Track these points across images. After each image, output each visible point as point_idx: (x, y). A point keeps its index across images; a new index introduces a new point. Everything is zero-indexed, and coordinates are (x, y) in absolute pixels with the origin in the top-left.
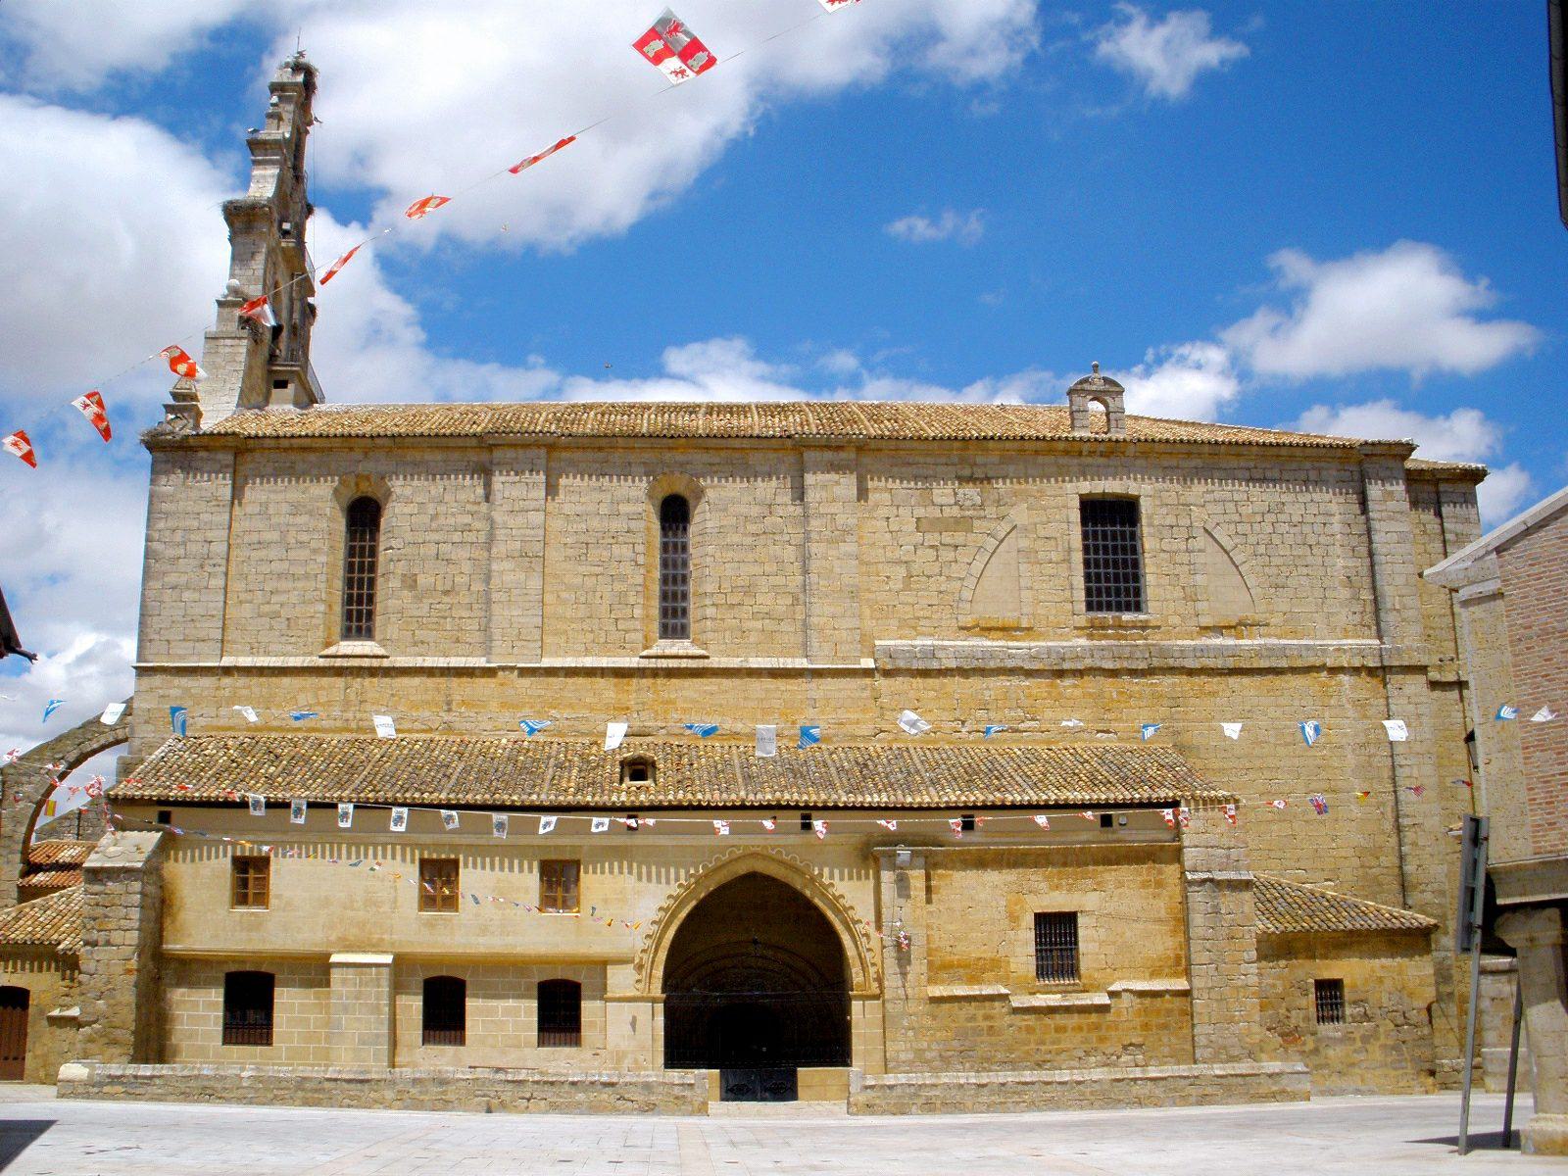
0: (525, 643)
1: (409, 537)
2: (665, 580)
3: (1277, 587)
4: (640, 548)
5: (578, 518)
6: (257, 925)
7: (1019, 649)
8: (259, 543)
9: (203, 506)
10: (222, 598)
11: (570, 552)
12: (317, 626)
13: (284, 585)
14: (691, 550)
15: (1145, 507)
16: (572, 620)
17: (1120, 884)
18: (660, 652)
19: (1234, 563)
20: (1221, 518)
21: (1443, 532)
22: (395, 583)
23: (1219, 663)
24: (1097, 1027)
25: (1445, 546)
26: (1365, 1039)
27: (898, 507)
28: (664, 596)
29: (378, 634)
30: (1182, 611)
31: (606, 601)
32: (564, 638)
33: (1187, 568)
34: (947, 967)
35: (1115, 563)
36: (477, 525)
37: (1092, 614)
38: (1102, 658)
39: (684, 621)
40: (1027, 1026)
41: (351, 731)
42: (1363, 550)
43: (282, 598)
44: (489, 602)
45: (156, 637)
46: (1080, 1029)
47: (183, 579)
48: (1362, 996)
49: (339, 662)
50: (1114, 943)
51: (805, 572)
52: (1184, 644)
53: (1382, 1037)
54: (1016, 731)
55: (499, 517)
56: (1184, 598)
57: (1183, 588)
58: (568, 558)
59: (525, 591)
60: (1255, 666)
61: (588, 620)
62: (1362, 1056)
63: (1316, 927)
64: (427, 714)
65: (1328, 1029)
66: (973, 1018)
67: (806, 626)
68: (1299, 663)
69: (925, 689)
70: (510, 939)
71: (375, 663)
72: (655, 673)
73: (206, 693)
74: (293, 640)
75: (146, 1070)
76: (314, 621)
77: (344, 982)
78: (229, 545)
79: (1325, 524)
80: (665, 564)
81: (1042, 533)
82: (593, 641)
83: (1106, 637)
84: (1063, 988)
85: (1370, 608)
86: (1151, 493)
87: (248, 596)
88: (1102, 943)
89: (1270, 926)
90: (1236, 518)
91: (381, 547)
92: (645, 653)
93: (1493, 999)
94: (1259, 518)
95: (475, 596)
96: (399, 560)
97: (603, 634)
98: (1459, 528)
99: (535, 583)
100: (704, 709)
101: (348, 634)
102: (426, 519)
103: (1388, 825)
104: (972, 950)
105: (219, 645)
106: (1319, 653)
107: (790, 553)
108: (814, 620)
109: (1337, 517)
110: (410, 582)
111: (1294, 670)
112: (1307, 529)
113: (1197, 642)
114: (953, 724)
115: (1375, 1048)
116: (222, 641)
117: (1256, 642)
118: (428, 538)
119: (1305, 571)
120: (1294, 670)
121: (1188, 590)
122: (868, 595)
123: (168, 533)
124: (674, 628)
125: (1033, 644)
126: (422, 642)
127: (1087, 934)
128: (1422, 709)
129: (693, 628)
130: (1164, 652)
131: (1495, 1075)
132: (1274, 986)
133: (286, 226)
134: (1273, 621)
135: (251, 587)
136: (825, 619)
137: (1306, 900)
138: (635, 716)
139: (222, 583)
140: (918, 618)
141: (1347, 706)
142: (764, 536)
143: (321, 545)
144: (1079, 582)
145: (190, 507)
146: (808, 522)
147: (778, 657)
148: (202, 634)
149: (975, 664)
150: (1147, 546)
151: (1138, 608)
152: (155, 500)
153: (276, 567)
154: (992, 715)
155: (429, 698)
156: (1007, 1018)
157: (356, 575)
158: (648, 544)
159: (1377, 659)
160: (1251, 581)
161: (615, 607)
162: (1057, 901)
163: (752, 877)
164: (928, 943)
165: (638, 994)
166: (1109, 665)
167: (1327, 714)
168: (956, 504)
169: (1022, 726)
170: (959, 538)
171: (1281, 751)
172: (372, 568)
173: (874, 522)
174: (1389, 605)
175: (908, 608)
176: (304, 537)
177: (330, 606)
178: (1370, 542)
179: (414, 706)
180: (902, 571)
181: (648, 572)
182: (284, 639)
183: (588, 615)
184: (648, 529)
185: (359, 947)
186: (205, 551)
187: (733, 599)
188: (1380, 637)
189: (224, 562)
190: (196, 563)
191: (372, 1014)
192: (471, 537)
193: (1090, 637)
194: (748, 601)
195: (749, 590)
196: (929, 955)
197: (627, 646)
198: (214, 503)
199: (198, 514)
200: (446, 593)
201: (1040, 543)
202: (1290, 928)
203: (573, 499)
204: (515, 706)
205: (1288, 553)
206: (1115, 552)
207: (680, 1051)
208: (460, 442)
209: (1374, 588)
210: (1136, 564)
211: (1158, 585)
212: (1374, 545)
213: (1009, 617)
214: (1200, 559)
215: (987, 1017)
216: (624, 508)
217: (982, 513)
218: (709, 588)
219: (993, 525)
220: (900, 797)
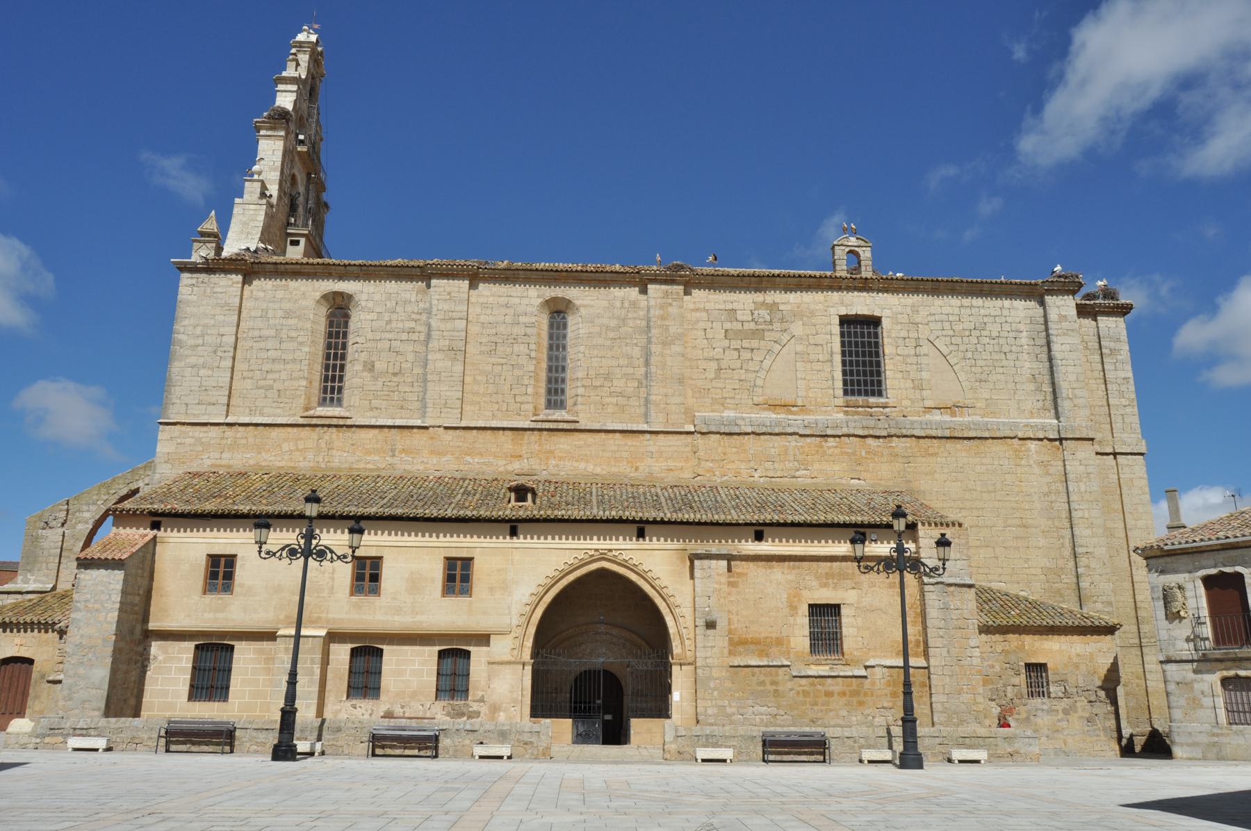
0: (449, 410)
1: (370, 336)
2: (550, 369)
3: (981, 381)
4: (533, 347)
5: (489, 325)
7: (796, 421)
8: (260, 337)
10: (229, 374)
12: (300, 396)
13: (277, 367)
14: (569, 349)
17: (873, 585)
18: (545, 418)
20: (940, 333)
21: (1101, 348)
22: (359, 367)
24: (855, 693)
25: (1102, 358)
26: (1066, 712)
27: (712, 322)
28: (549, 381)
29: (345, 403)
30: (912, 397)
32: (477, 407)
33: (915, 367)
34: (743, 642)
35: (864, 363)
36: (419, 328)
37: (849, 398)
39: (563, 398)
40: (803, 691)
42: (1044, 356)
43: (276, 376)
44: (425, 381)
45: (178, 401)
46: (844, 694)
47: (201, 360)
48: (1063, 677)
49: (314, 421)
50: (868, 629)
51: (647, 364)
52: (918, 421)
53: (1080, 710)
54: (794, 477)
55: (434, 323)
56: (913, 388)
57: (913, 380)
58: (481, 353)
61: (495, 395)
62: (1064, 724)
63: (1025, 623)
64: (377, 458)
65: (1037, 702)
66: (762, 683)
67: (647, 401)
69: (729, 446)
70: (419, 618)
71: (341, 422)
73: (212, 442)
74: (282, 405)
76: (298, 393)
78: (237, 339)
80: (550, 359)
81: (812, 341)
82: (498, 410)
84: (831, 662)
85: (1050, 397)
86: (891, 315)
87: (250, 374)
88: (859, 628)
89: (989, 620)
90: (951, 333)
91: (350, 343)
92: (534, 419)
93: (1178, 683)
94: (967, 333)
95: (416, 377)
96: (362, 351)
97: (505, 404)
98: (1112, 345)
99: (459, 368)
100: (573, 457)
101: (323, 402)
102: (383, 324)
103: (1067, 552)
104: (761, 631)
105: (225, 407)
107: (637, 352)
108: (653, 398)
109: (1025, 334)
112: (1002, 341)
114: (749, 471)
115: (1074, 717)
116: (228, 405)
117: (966, 419)
118: (383, 337)
119: (1001, 370)
121: (916, 382)
122: (691, 382)
123: (191, 328)
124: (556, 402)
125: (805, 417)
126: (377, 408)
127: (849, 625)
128: (1090, 469)
129: (569, 403)
131: (1182, 745)
132: (993, 667)
133: (301, 137)
134: (978, 405)
135: (252, 368)
136: (660, 397)
137: (1014, 602)
138: (526, 461)
139: (229, 364)
140: (726, 398)
141: (1034, 466)
142: (619, 341)
143: (305, 340)
144: (838, 375)
146: (650, 331)
147: (627, 423)
148: (213, 400)
150: (887, 351)
151: (880, 394)
154: (776, 465)
156: (789, 683)
157: (331, 362)
158: (538, 344)
159: (1056, 433)
160: (962, 377)
162: (825, 596)
163: (603, 574)
164: (729, 624)
165: (513, 659)
166: (861, 432)
167: (1019, 471)
169: (797, 474)
170: (755, 344)
172: (343, 357)
173: (695, 332)
174: (1064, 395)
175: (719, 391)
176: (294, 334)
177: (311, 382)
178: (1050, 350)
179: (368, 453)
180: (714, 365)
181: (538, 363)
182: (274, 405)
184: (539, 334)
186: (219, 341)
188: (1058, 418)
189: (232, 349)
190: (210, 349)
192: (414, 337)
193: (846, 413)
194: (607, 384)
195: (608, 377)
196: (730, 633)
197: (522, 413)
198: (227, 308)
199: (215, 315)
200: (395, 374)
201: (811, 348)
202: (1005, 623)
204: (441, 453)
205: (989, 358)
206: (864, 356)
207: (542, 706)
209: (1053, 384)
210: (878, 364)
211: (895, 378)
212: (1053, 353)
213: (789, 399)
214: (924, 360)
215: (774, 683)
216: (522, 319)
217: (770, 327)
218: (580, 374)
219: (779, 335)
220: (710, 515)
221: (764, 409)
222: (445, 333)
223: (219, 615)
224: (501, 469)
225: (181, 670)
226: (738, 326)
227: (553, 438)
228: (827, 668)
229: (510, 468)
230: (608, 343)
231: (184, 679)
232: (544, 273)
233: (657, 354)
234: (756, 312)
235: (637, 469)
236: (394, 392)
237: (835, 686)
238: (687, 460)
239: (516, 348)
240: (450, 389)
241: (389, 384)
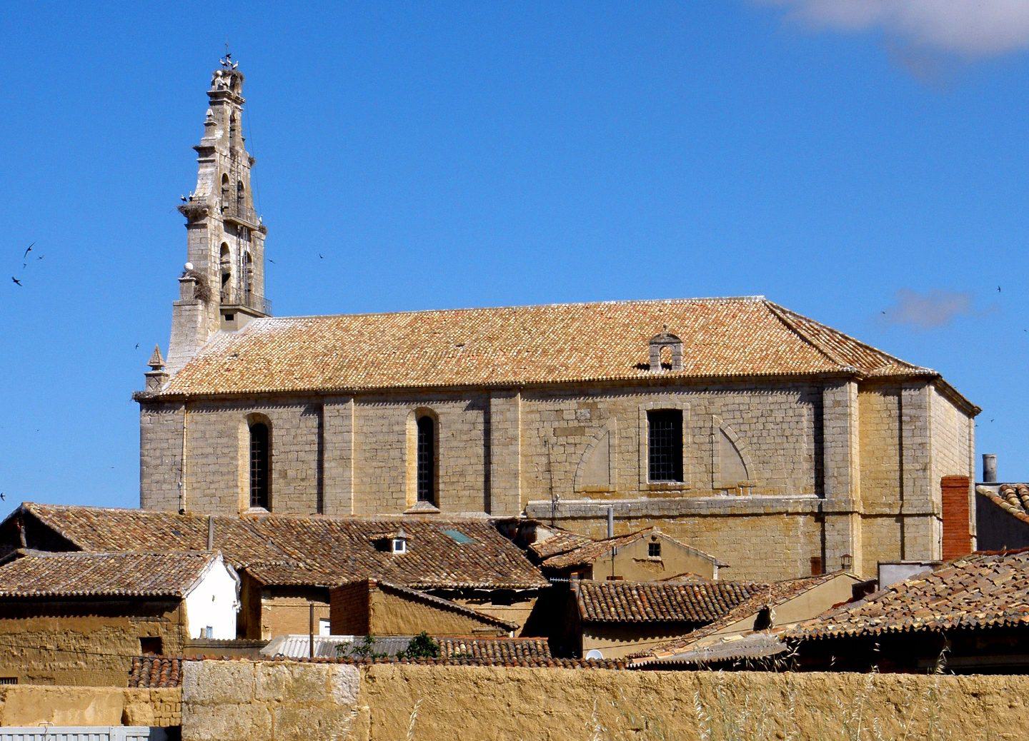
7: (605, 503)
9: (170, 436)
15: (687, 416)
16: (369, 493)
19: (736, 449)
23: (722, 511)
27: (544, 422)
31: (387, 482)
38: (653, 509)
43: (217, 485)
56: (706, 472)
57: (705, 465)
59: (342, 479)
68: (771, 510)
75: (654, 558)
79: (797, 422)
83: (658, 496)
87: (199, 485)
94: (755, 420)
98: (913, 412)
106: (784, 504)
112: (785, 426)
113: (711, 498)
119: (782, 452)
125: (615, 501)
130: (688, 504)
145: (164, 436)
149: (581, 514)
152: (143, 432)
153: (212, 468)
161: (391, 485)
166: (656, 513)
170: (577, 439)
171: (758, 563)
174: (830, 474)
176: (226, 451)
187: (455, 479)
193: (649, 496)
195: (462, 474)
199: (168, 439)
200: (303, 480)
203: (369, 423)
217: (590, 424)
221: (584, 496)
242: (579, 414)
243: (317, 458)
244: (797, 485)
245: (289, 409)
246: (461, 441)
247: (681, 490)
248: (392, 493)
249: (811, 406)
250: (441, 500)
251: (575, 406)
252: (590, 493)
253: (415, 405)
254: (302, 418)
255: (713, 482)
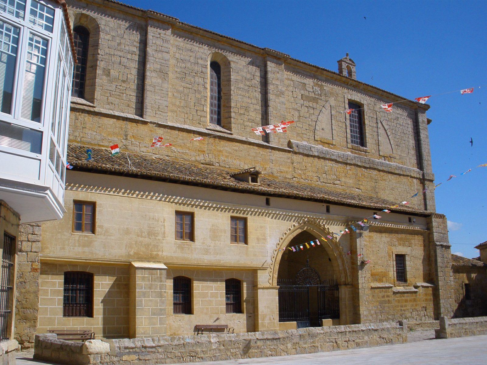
0: (161, 113)
1: (107, 50)
6: (89, 244)
11: (178, 75)
16: (179, 107)
41: (78, 142)
54: (335, 184)
60: (395, 172)
68: (405, 174)
70: (218, 257)
72: (215, 137)
77: (143, 279)
82: (187, 118)
96: (102, 61)
110: (107, 72)
111: (404, 175)
120: (404, 175)
126: (112, 103)
134: (397, 157)
138: (207, 155)
140: (303, 134)
155: (117, 131)
166: (359, 164)
168: (313, 91)
180: (296, 114)
183: (185, 105)
185: (146, 258)
187: (242, 111)
191: (158, 297)
193: (352, 152)
197: (201, 123)
200: (124, 81)
203: (180, 52)
208: (134, 12)
222: (157, 60)
223: (86, 249)
224: (193, 159)
225: (55, 292)
226: (307, 94)
227: (222, 142)
228: (402, 288)
229: (198, 158)
230: (246, 88)
231: (59, 299)
232: (214, 35)
233: (273, 100)
234: (314, 87)
235: (265, 169)
236: (123, 94)
237: (407, 297)
238: (289, 168)
239: (197, 79)
240: (161, 98)
241: (120, 87)
242: (314, 89)
243: (137, 67)
244: (411, 162)
245: (116, 20)
246: (245, 85)
247: (366, 152)
248: (197, 110)
249: (411, 120)
250: (233, 125)
251: (312, 84)
252: (323, 143)
253: (214, 49)
254: (126, 31)
255: (379, 151)
